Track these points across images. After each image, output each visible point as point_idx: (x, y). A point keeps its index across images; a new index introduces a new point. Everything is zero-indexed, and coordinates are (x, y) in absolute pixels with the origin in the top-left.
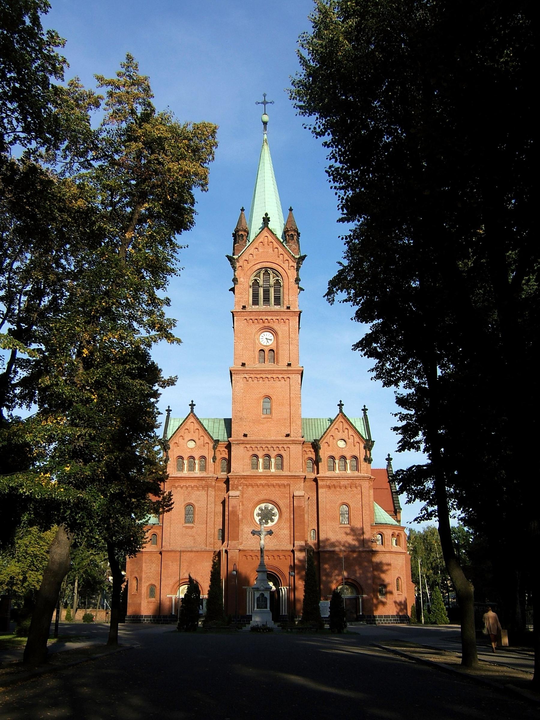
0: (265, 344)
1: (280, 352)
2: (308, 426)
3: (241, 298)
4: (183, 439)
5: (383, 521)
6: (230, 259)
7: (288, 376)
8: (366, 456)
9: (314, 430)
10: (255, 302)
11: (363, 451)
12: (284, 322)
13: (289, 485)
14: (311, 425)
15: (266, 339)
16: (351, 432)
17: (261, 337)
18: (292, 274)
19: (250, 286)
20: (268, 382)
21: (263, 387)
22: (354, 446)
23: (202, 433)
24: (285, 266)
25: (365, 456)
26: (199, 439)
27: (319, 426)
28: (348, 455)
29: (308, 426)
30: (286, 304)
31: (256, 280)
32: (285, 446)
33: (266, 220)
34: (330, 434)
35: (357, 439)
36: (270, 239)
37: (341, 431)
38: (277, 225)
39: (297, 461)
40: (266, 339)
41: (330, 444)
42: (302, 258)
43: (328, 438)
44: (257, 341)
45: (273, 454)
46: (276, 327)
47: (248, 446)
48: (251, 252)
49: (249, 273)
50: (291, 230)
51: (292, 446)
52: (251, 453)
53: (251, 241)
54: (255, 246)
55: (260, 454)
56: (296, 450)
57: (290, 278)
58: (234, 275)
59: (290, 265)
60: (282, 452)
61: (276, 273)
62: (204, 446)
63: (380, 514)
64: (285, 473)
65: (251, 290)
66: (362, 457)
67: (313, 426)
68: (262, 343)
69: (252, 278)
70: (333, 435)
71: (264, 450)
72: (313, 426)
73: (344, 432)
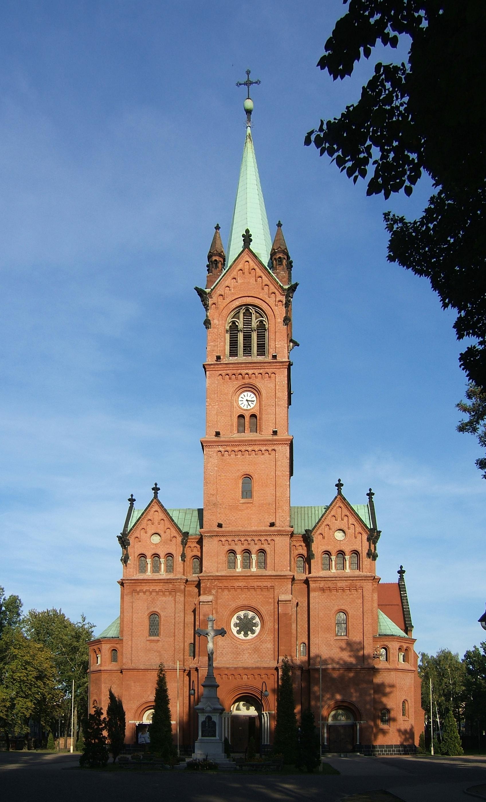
0: (245, 408)
1: (264, 417)
2: (299, 515)
3: (215, 346)
4: (146, 533)
5: (389, 632)
6: (201, 293)
7: (273, 448)
8: (370, 550)
9: (306, 521)
10: (233, 353)
11: (366, 544)
12: (270, 377)
13: (273, 587)
14: (303, 516)
15: (246, 401)
16: (352, 520)
17: (240, 399)
18: (280, 311)
19: (227, 331)
20: (248, 456)
21: (242, 464)
22: (355, 537)
23: (168, 524)
24: (271, 301)
25: (369, 550)
26: (165, 532)
27: (313, 515)
28: (347, 549)
29: (299, 515)
30: (272, 352)
31: (234, 323)
32: (269, 539)
33: (247, 238)
34: (325, 523)
35: (359, 529)
36: (252, 264)
37: (339, 519)
38: (262, 248)
39: (282, 556)
40: (246, 401)
41: (325, 535)
42: (293, 288)
43: (322, 529)
44: (235, 404)
45: (254, 549)
46: (259, 383)
47: (223, 539)
48: (227, 284)
49: (225, 312)
50: (279, 252)
51: (277, 539)
52: (227, 548)
53: (229, 266)
54: (232, 276)
55: (238, 549)
56: (282, 543)
57: (277, 317)
58: (207, 316)
59: (278, 299)
60: (266, 547)
61: (260, 312)
62: (171, 541)
63: (385, 624)
64: (269, 572)
65: (228, 336)
66: (365, 552)
67: (306, 515)
68: (242, 406)
69: (229, 320)
70: (329, 523)
71: (242, 544)
72: (306, 515)
73: (342, 520)
